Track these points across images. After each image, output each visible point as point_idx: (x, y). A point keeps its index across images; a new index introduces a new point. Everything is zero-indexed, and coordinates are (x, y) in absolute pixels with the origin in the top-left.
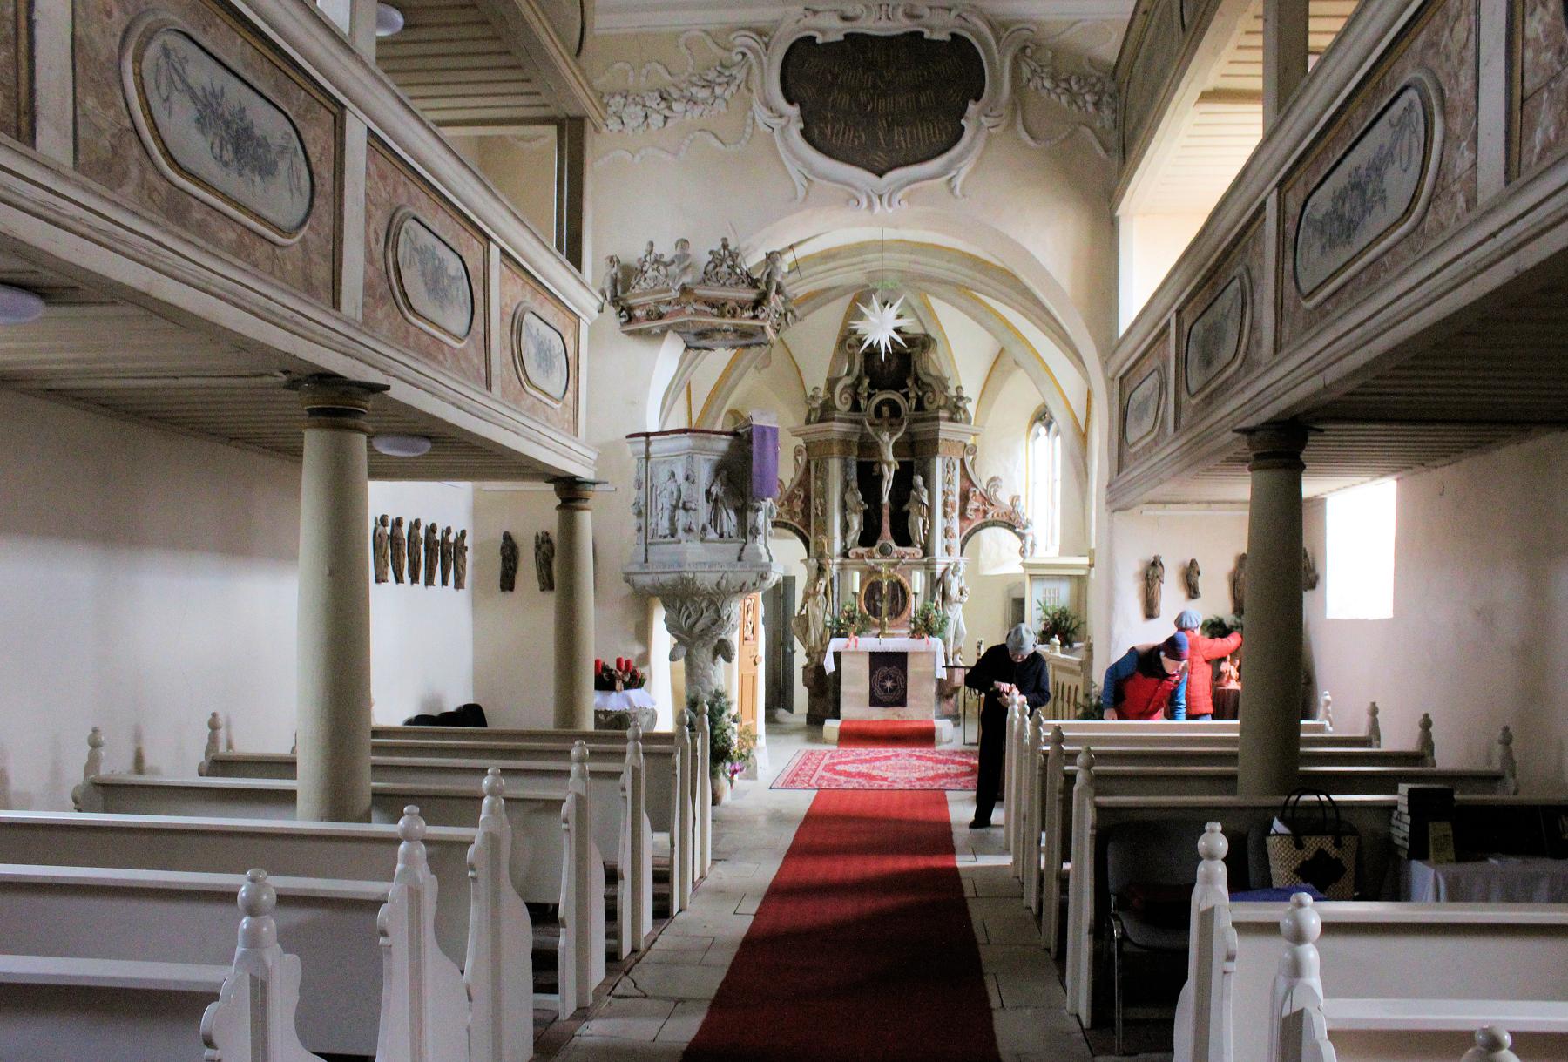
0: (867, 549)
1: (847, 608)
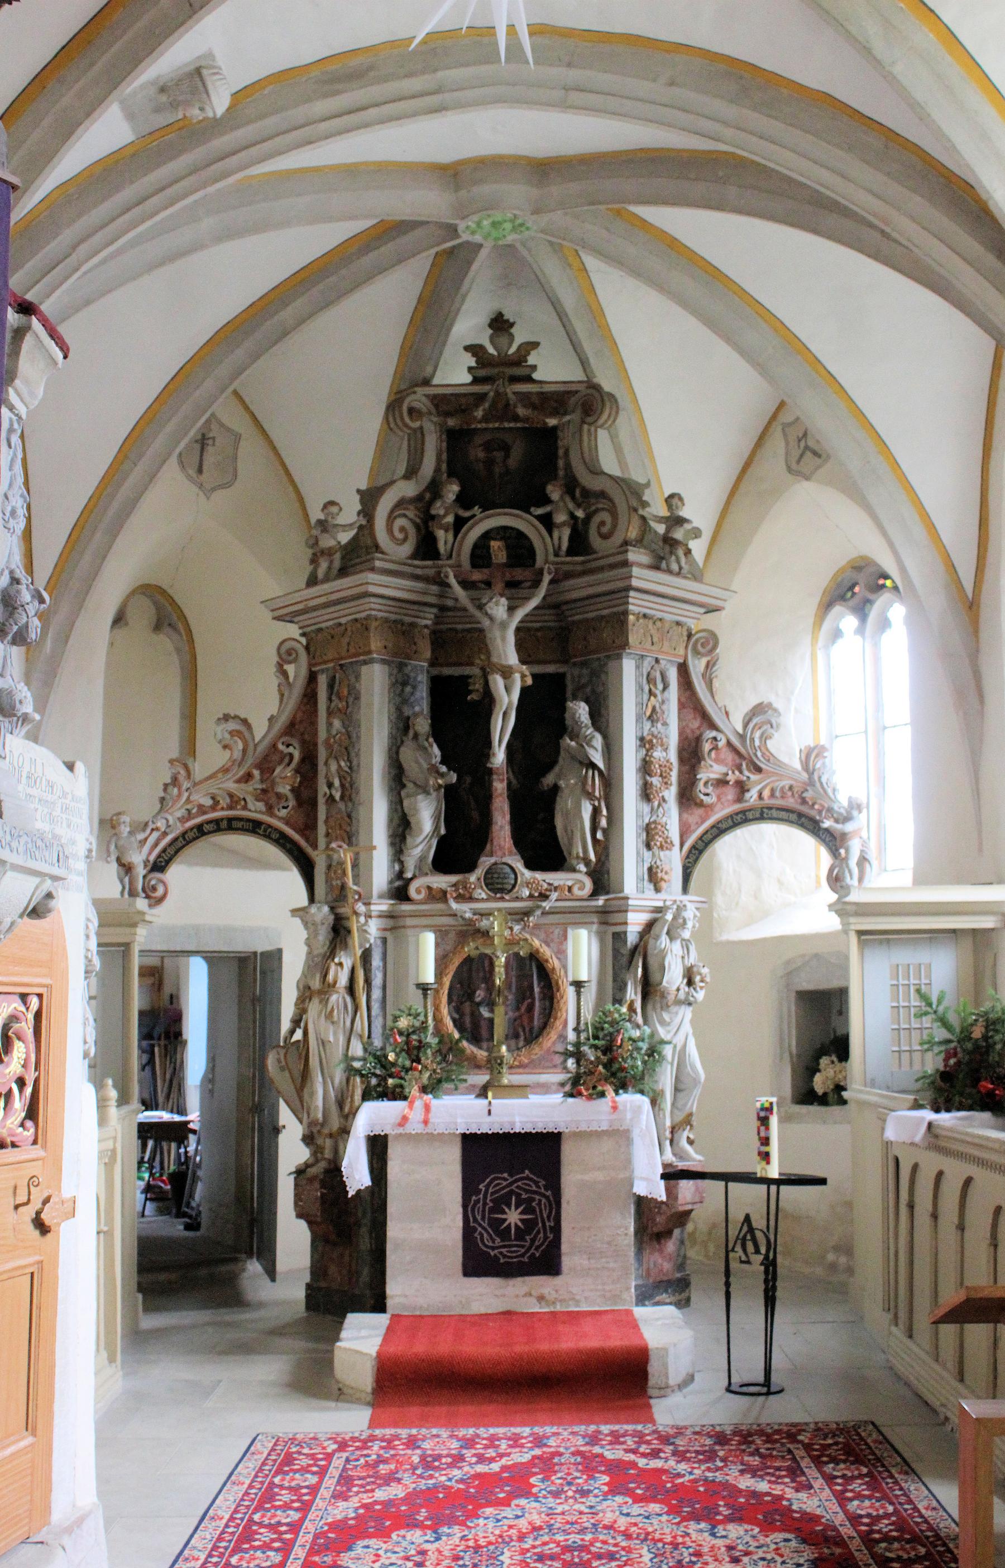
0: (453, 878)
1: (403, 1023)
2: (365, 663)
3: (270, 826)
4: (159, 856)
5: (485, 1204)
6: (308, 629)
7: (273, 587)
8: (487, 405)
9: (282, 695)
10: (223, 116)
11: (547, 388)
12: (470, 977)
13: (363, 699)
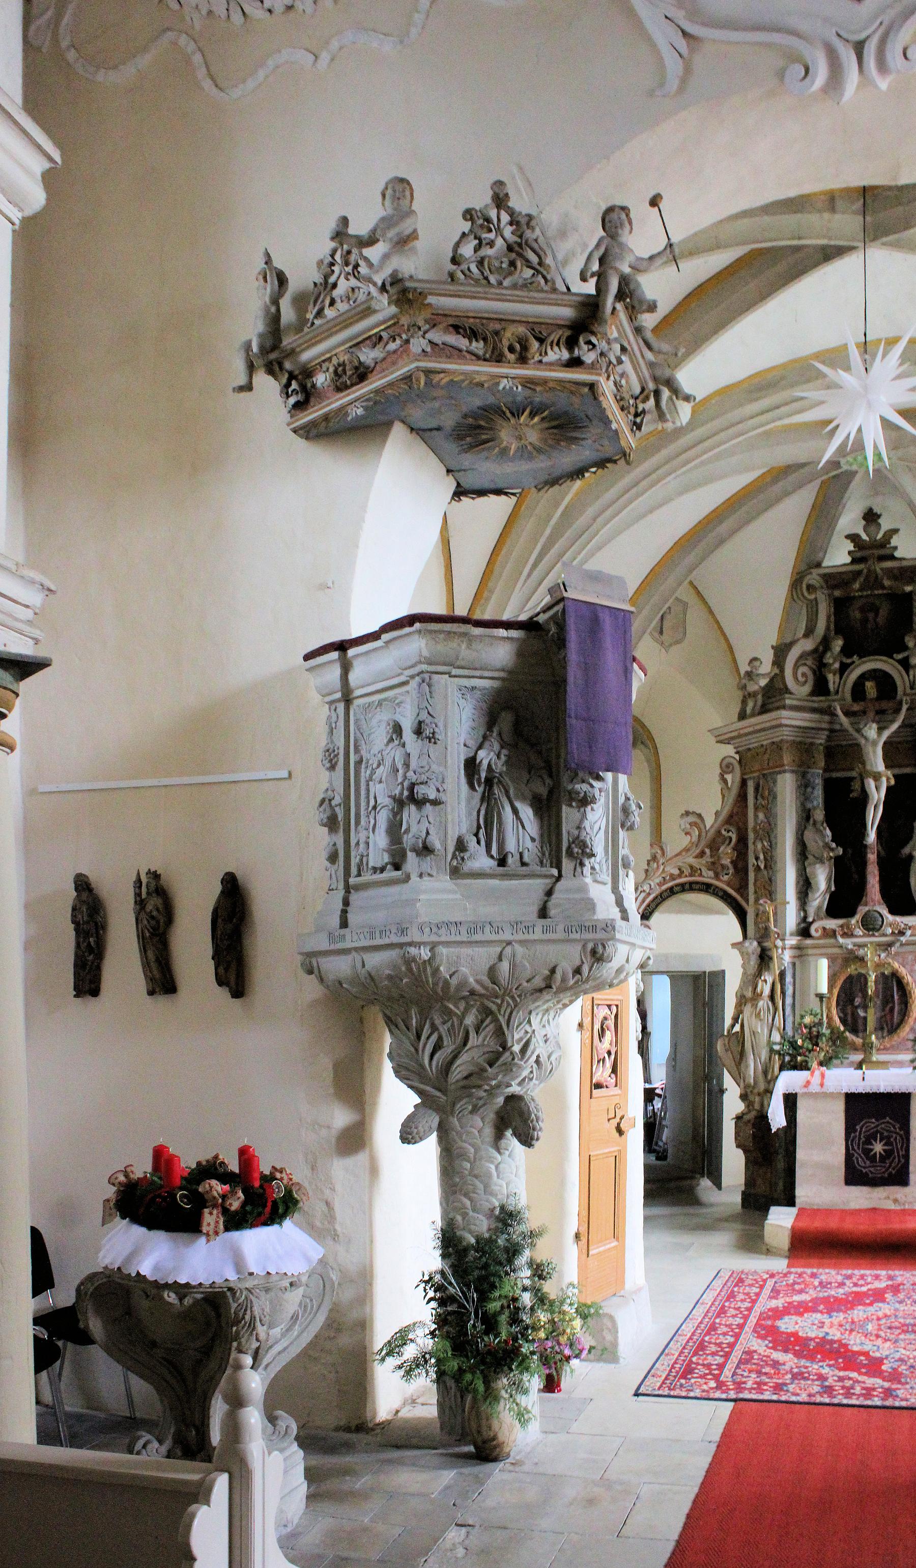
0: (840, 922)
1: (808, 1020)
2: (780, 773)
3: (717, 887)
4: (645, 909)
5: (860, 1139)
6: (740, 749)
7: (717, 722)
8: (862, 579)
9: (723, 796)
10: (688, 424)
11: (905, 563)
12: (851, 989)
13: (779, 798)
